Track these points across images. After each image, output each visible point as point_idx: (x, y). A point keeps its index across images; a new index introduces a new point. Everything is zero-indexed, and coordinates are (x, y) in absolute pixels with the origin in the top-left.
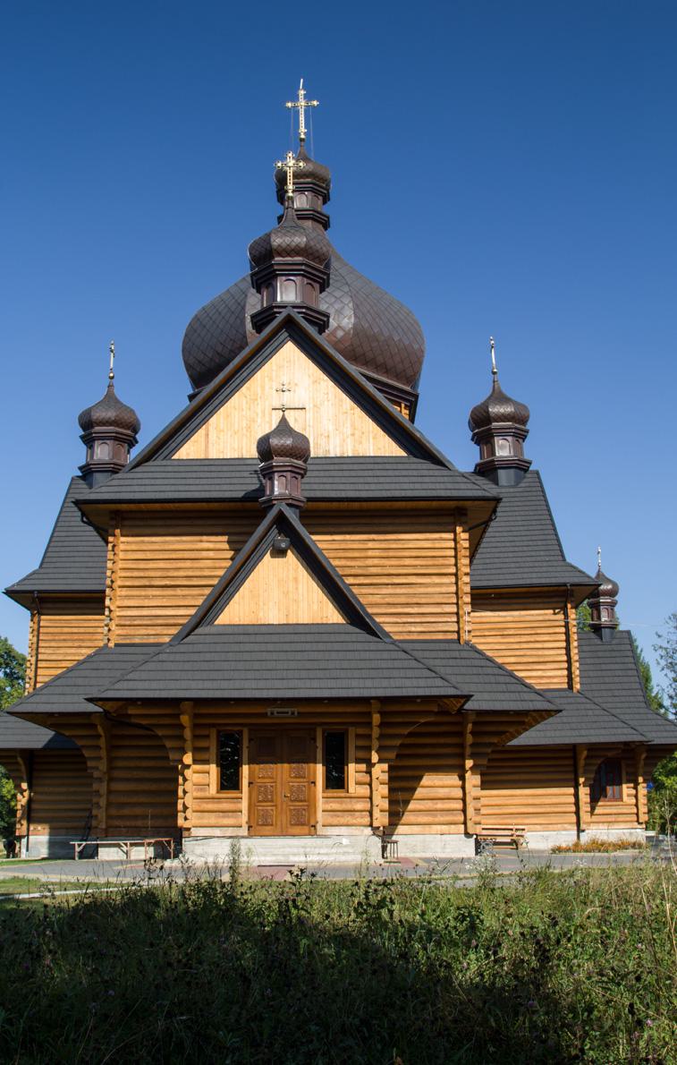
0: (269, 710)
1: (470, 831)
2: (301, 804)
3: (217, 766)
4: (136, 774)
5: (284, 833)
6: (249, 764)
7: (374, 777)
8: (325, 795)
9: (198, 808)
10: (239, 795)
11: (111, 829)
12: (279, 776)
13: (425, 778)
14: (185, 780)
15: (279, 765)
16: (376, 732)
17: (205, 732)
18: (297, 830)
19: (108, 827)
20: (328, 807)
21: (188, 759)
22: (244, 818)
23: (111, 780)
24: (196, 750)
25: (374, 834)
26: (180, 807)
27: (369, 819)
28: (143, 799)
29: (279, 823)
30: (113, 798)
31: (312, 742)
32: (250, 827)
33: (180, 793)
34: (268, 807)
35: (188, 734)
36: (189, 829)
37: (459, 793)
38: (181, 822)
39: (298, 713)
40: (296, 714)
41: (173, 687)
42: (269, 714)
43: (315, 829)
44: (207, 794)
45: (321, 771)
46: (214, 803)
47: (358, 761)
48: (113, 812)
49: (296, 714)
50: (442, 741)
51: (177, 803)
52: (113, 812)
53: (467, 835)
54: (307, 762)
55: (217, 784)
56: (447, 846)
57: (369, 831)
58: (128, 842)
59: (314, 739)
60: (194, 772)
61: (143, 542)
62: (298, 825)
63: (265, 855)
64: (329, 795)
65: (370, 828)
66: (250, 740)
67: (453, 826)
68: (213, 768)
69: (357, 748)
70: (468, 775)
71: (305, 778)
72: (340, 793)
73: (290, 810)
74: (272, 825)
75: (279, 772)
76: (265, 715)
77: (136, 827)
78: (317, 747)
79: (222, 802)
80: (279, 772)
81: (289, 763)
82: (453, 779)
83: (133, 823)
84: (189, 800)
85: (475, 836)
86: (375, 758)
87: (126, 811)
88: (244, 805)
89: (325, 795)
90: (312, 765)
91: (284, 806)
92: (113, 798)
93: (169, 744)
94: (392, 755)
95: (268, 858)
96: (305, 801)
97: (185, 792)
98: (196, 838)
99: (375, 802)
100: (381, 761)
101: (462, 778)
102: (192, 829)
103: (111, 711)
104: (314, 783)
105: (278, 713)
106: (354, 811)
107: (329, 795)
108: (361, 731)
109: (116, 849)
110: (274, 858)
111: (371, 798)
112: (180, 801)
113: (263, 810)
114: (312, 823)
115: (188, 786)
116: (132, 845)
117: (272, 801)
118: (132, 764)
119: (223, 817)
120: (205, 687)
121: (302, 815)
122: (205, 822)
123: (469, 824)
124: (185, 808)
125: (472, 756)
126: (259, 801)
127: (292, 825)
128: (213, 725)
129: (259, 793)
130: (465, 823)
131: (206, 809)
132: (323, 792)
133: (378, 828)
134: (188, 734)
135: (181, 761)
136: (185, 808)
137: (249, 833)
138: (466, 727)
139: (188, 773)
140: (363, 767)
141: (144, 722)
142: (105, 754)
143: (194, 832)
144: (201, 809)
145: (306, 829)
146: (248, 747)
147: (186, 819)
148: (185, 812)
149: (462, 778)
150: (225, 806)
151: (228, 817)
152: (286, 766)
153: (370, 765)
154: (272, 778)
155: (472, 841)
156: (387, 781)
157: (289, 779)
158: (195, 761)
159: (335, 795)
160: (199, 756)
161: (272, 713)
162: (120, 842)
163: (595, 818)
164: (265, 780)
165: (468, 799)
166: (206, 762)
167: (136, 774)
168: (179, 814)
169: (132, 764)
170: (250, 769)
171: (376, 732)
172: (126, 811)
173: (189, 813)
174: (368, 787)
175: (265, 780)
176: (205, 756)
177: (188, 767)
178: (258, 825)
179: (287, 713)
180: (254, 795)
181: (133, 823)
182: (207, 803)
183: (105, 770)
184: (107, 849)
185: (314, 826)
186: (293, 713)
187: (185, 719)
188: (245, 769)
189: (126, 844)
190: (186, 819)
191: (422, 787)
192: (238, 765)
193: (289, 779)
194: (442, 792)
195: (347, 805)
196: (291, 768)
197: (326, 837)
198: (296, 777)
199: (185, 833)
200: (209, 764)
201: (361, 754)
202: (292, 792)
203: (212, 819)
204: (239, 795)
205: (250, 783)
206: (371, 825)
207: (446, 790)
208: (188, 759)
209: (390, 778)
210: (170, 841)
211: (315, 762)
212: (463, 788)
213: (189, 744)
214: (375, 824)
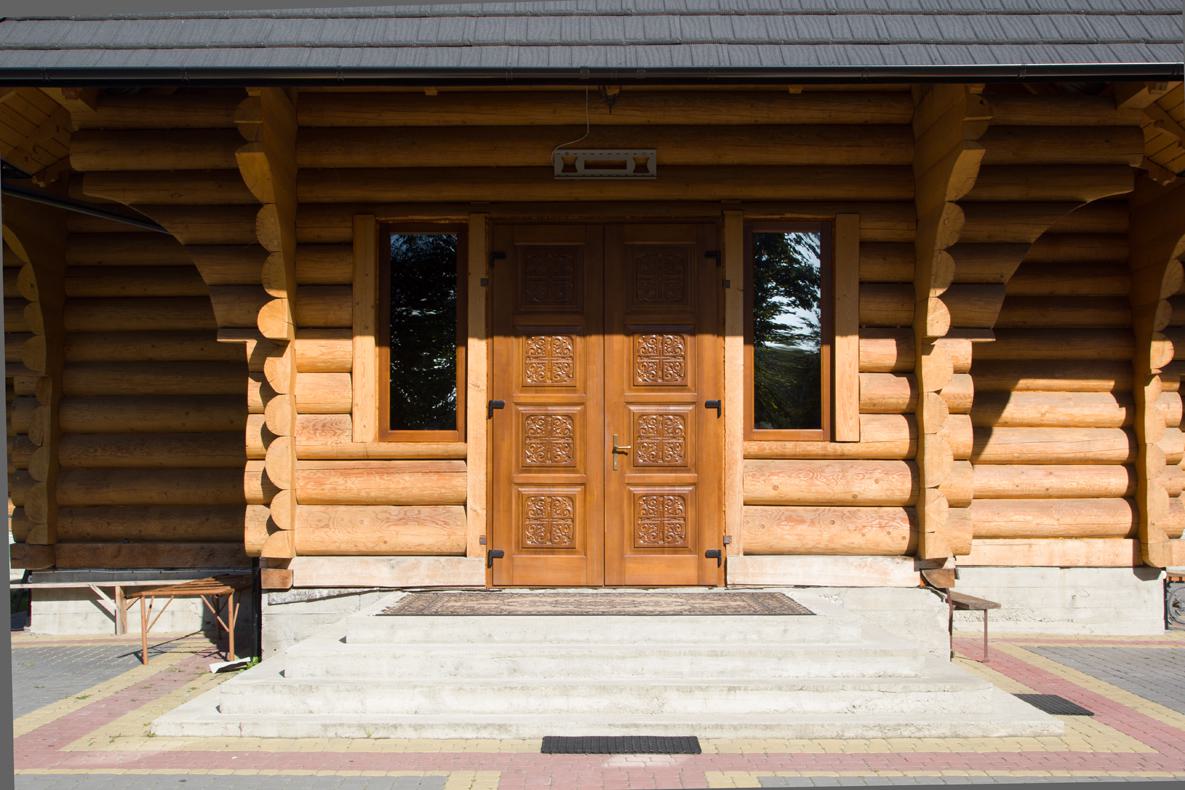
0: (558, 157)
1: (1155, 558)
2: (671, 476)
3: (379, 343)
4: (143, 383)
5: (612, 579)
6: (490, 333)
7: (928, 386)
8: (754, 447)
9: (312, 491)
10: (456, 447)
11: (67, 547)
12: (594, 383)
13: (1015, 396)
14: (268, 393)
15: (595, 340)
16: (950, 225)
17: (338, 231)
18: (656, 566)
19: (59, 540)
20: (762, 489)
21: (275, 319)
22: (472, 526)
23: (64, 399)
24: (303, 293)
25: (926, 584)
26: (252, 487)
27: (904, 528)
28: (161, 457)
29: (594, 543)
30: (74, 456)
31: (711, 262)
32: (492, 557)
33: (253, 439)
34: (556, 486)
35: (270, 229)
36: (282, 564)
37: (1120, 445)
38: (254, 537)
39: (660, 167)
40: (652, 168)
41: (204, 38)
42: (558, 169)
43: (722, 564)
44: (344, 444)
45: (740, 361)
46: (370, 472)
47: (870, 330)
48: (75, 495)
49: (652, 168)
50: (1064, 287)
51: (241, 470)
52: (75, 495)
53: (1143, 568)
54: (695, 331)
55: (381, 409)
56: (1079, 602)
57: (906, 572)
58: (117, 585)
59: (717, 256)
60: (302, 369)
61: (558, 594)
62: (662, 549)
63: (566, 690)
64: (769, 447)
65: (910, 563)
66: (494, 256)
67: (1099, 543)
68: (365, 353)
69: (867, 286)
70: (1152, 390)
71: (683, 387)
72: (808, 441)
73: (634, 498)
74: (571, 549)
75: (596, 368)
76: (543, 173)
77: (141, 540)
78: (726, 284)
79: (401, 471)
80: (596, 368)
81: (628, 333)
82: (1098, 402)
83: (133, 528)
84: (278, 462)
85: (1163, 575)
86: (938, 317)
87: (113, 495)
88: (473, 480)
89: (754, 447)
90: (708, 340)
91: (613, 487)
92: (74, 456)
93: (212, 272)
94: (989, 312)
95: (580, 702)
96: (684, 468)
97: (268, 437)
98: (311, 593)
99: (931, 476)
100: (955, 331)
101: (1130, 398)
102: (296, 564)
103: (31, 168)
104: (716, 406)
105: (588, 166)
106: (855, 503)
107: (769, 447)
108: (877, 229)
109: (86, 605)
110: (603, 702)
111: (914, 460)
112: (252, 469)
113: (537, 498)
114: (711, 544)
115: (278, 414)
116: (128, 593)
117: (571, 468)
118: (130, 352)
119: (403, 521)
120: (327, 37)
121: (674, 515)
122: (338, 538)
123: (1155, 538)
124: (270, 490)
125: (1169, 333)
126: (527, 469)
127: (637, 548)
128: (365, 208)
129: (526, 436)
130: (1137, 534)
131: (341, 495)
132: (747, 437)
133: (940, 562)
134: (270, 229)
135: (253, 330)
136: (270, 490)
137: (491, 576)
138: (774, 351)
139: (277, 369)
140: (885, 350)
141: (127, 198)
142: (40, 318)
143: (302, 571)
144: (327, 491)
145: (687, 565)
146: (484, 282)
147: (272, 527)
148: (268, 505)
149: (1130, 398)
150: (409, 482)
151: (419, 521)
152: (618, 342)
153: (913, 343)
154: (572, 388)
155: (1156, 585)
156: (968, 402)
157: (631, 395)
158: (302, 330)
159: (789, 447)
160: (315, 314)
161: (570, 167)
162: (94, 586)
163: (985, 478)
164: (541, 397)
165: (1153, 463)
166: (344, 331)
167: (143, 383)
168: (249, 509)
169: (130, 352)
170: (491, 354)
171: (950, 225)
172: (113, 495)
173: (281, 508)
174: (902, 421)
175: (541, 397)
176: (339, 314)
177: (278, 347)
178: (523, 548)
179: (623, 166)
180: (508, 446)
181: (133, 528)
182: (345, 473)
183: (43, 371)
184: (55, 605)
185: (716, 555)
186: (641, 168)
187: (255, 168)
188: (477, 350)
189: (110, 592)
190: (272, 527)
191: (1006, 424)
192: (452, 337)
193: (631, 395)
194: (1066, 443)
195: (830, 481)
196: (635, 352)
197: (771, 604)
198: (652, 386)
199: (270, 577)
200: (351, 337)
201: (883, 309)
202: (637, 436)
203: (364, 528)
204: (456, 447)
205: (493, 407)
206: (914, 552)
207: (1079, 435)
208: (275, 319)
209: (978, 394)
210: (225, 596)
211: (720, 330)
212: (1133, 429)
213: (276, 265)
214: (931, 552)
